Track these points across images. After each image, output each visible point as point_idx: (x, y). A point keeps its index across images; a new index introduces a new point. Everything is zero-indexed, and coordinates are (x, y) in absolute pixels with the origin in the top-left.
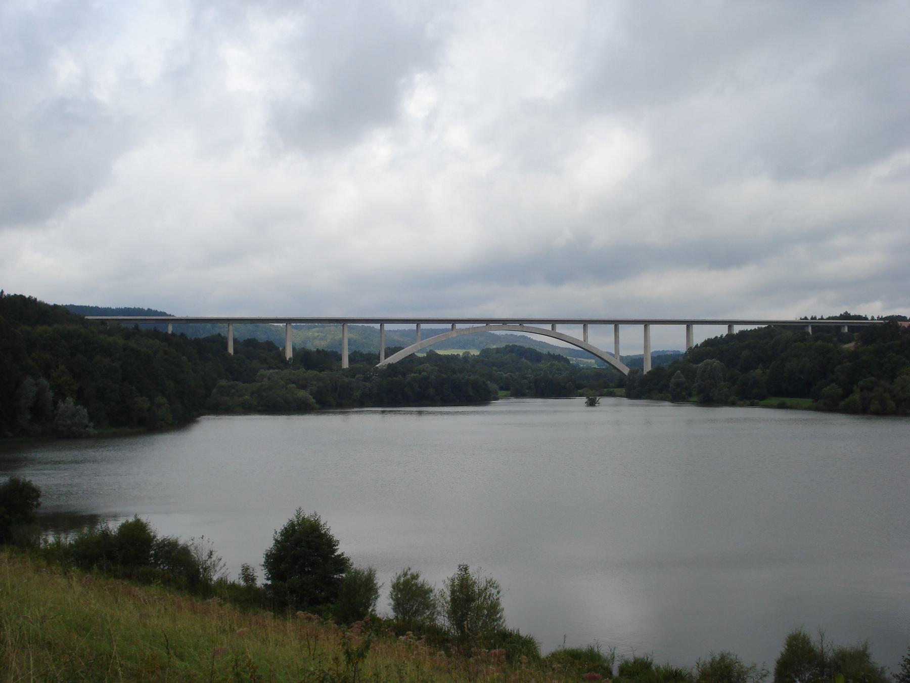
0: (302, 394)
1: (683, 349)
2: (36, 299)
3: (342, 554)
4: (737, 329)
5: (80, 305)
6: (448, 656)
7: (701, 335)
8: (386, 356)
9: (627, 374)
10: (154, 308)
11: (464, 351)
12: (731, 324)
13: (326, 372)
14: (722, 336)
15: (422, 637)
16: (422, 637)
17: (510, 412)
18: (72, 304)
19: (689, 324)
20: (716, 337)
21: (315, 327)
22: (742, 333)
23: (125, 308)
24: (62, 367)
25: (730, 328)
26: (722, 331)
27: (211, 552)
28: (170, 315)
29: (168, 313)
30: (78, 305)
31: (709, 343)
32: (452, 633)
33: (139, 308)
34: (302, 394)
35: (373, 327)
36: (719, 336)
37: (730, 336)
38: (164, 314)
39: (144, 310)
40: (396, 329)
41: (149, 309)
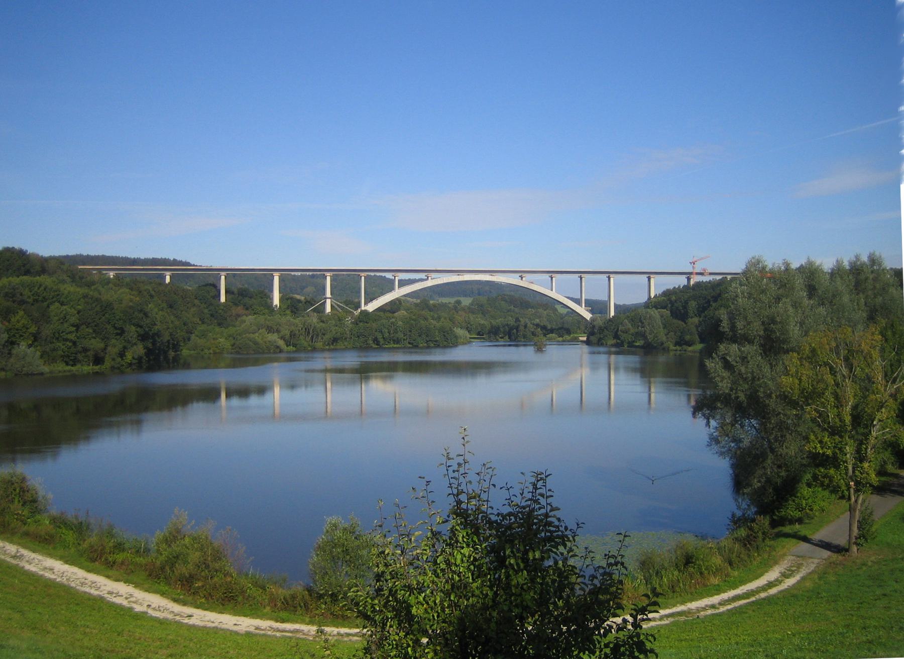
2: (787, 265)
4: (695, 279)
5: (100, 254)
6: (307, 301)
8: (369, 300)
9: (588, 319)
10: (179, 259)
11: (455, 299)
12: (689, 275)
13: (663, 612)
14: (679, 287)
19: (649, 274)
20: (675, 288)
21: (473, 342)
22: (698, 285)
25: (689, 279)
26: (682, 281)
28: (194, 265)
31: (667, 293)
32: (504, 553)
33: (165, 259)
35: (385, 276)
37: (687, 287)
38: (188, 264)
41: (174, 260)
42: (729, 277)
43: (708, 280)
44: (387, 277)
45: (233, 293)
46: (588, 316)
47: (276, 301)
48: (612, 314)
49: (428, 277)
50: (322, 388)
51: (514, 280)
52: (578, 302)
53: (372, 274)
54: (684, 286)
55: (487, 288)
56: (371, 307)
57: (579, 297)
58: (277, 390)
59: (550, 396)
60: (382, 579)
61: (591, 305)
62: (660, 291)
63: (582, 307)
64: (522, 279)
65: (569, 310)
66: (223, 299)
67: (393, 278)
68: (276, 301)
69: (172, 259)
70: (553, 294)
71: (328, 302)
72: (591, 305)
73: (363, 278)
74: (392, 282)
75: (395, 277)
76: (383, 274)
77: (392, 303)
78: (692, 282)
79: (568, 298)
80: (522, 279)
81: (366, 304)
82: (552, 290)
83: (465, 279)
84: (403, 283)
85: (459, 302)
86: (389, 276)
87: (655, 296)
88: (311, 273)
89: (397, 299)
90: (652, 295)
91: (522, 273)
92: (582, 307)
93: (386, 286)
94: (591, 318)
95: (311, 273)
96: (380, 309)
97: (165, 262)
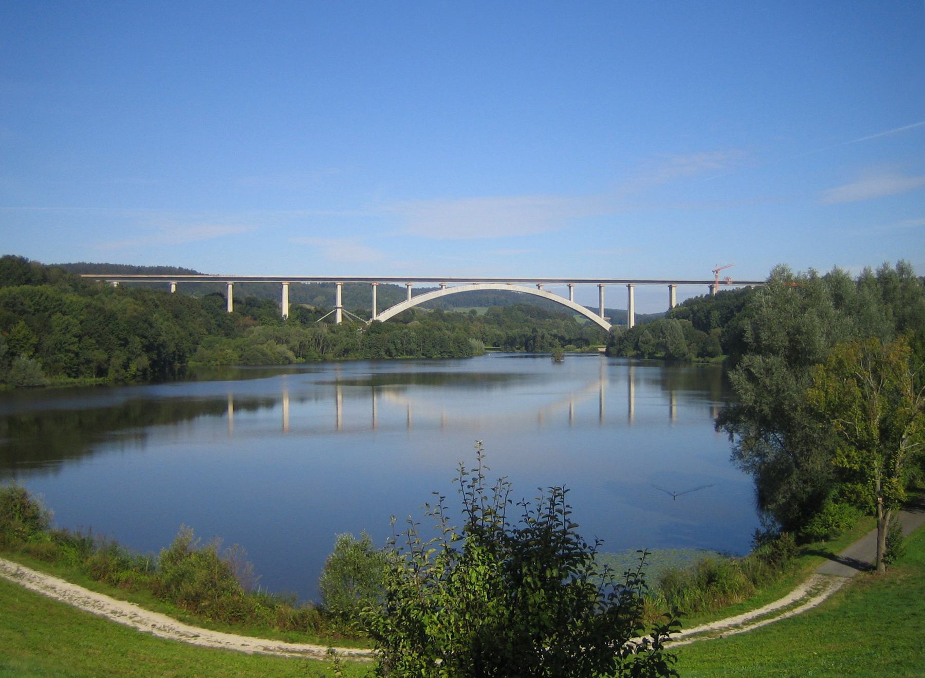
3: (799, 273)
5: (104, 263)
7: (679, 296)
8: (381, 309)
9: (608, 330)
10: (184, 267)
12: (711, 284)
14: (702, 296)
15: (549, 576)
16: (549, 576)
17: (512, 357)
22: (721, 294)
23: (158, 267)
24: (22, 323)
25: (711, 288)
26: (704, 290)
27: (91, 528)
28: (200, 274)
29: (198, 271)
31: (689, 303)
33: (171, 267)
36: (699, 296)
38: (194, 273)
39: (176, 268)
40: (420, 287)
41: (180, 268)
42: (753, 286)
45: (240, 303)
46: (607, 326)
47: (285, 311)
48: (633, 324)
49: (442, 286)
50: (333, 401)
51: (531, 289)
52: (597, 311)
53: (385, 283)
54: (707, 295)
55: (503, 298)
56: (384, 317)
57: (598, 307)
58: (286, 403)
59: (568, 410)
61: (611, 315)
62: (681, 301)
63: (601, 317)
64: (539, 288)
65: (588, 320)
66: (230, 309)
67: (406, 287)
68: (285, 311)
69: (178, 268)
70: (571, 304)
71: (339, 312)
72: (611, 315)
73: (375, 287)
74: (405, 291)
75: (408, 286)
78: (715, 292)
79: (587, 307)
80: (539, 288)
81: (378, 313)
82: (570, 300)
83: (481, 289)
84: (416, 293)
85: (474, 312)
86: (402, 285)
87: (677, 306)
88: (321, 282)
89: (410, 309)
91: (539, 282)
92: (601, 317)
93: (401, 295)
94: (611, 328)
95: (321, 282)
96: (393, 319)
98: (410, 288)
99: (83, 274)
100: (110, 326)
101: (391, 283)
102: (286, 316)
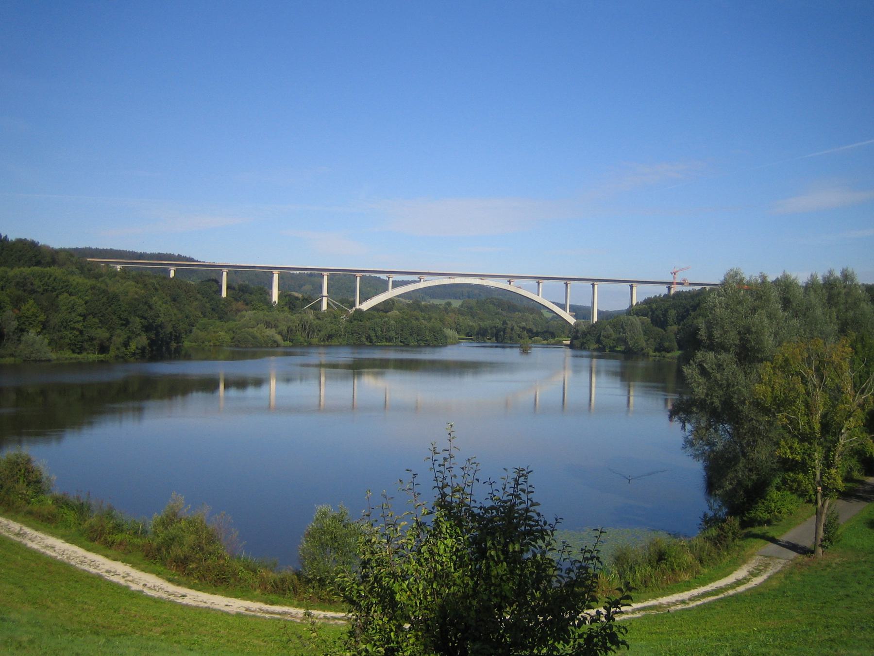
0: (271, 332)
1: (625, 306)
2: (764, 278)
4: (675, 289)
9: (572, 324)
10: (183, 254)
11: (446, 301)
12: (669, 284)
14: (660, 296)
18: (23, 237)
19: (632, 283)
22: (678, 294)
23: (159, 253)
24: (31, 302)
25: (669, 289)
26: (662, 290)
28: (197, 261)
29: (196, 259)
30: (82, 247)
31: (648, 302)
32: (486, 545)
33: (170, 254)
34: (271, 332)
38: (192, 260)
41: (189, 258)
42: (708, 288)
43: (684, 291)
44: (381, 278)
45: (234, 289)
46: (572, 321)
47: (275, 298)
48: (595, 319)
49: (420, 279)
50: (317, 382)
51: (502, 284)
52: (563, 307)
54: (665, 295)
55: (477, 291)
56: (366, 306)
57: (564, 303)
58: (273, 383)
60: (368, 566)
62: (642, 299)
63: (566, 312)
66: (224, 294)
67: (387, 279)
68: (275, 298)
69: (177, 255)
70: (539, 299)
71: (325, 300)
73: (358, 278)
76: (378, 275)
77: (386, 302)
78: (672, 292)
79: (553, 303)
82: (538, 295)
83: (456, 283)
84: (396, 284)
85: (449, 304)
88: (309, 272)
89: (390, 299)
90: (634, 303)
91: (510, 278)
92: (566, 312)
93: (382, 286)
95: (309, 272)
96: (373, 308)
97: (170, 257)
98: (391, 280)
99: (89, 258)
100: (113, 307)
101: (373, 275)
102: (275, 302)
